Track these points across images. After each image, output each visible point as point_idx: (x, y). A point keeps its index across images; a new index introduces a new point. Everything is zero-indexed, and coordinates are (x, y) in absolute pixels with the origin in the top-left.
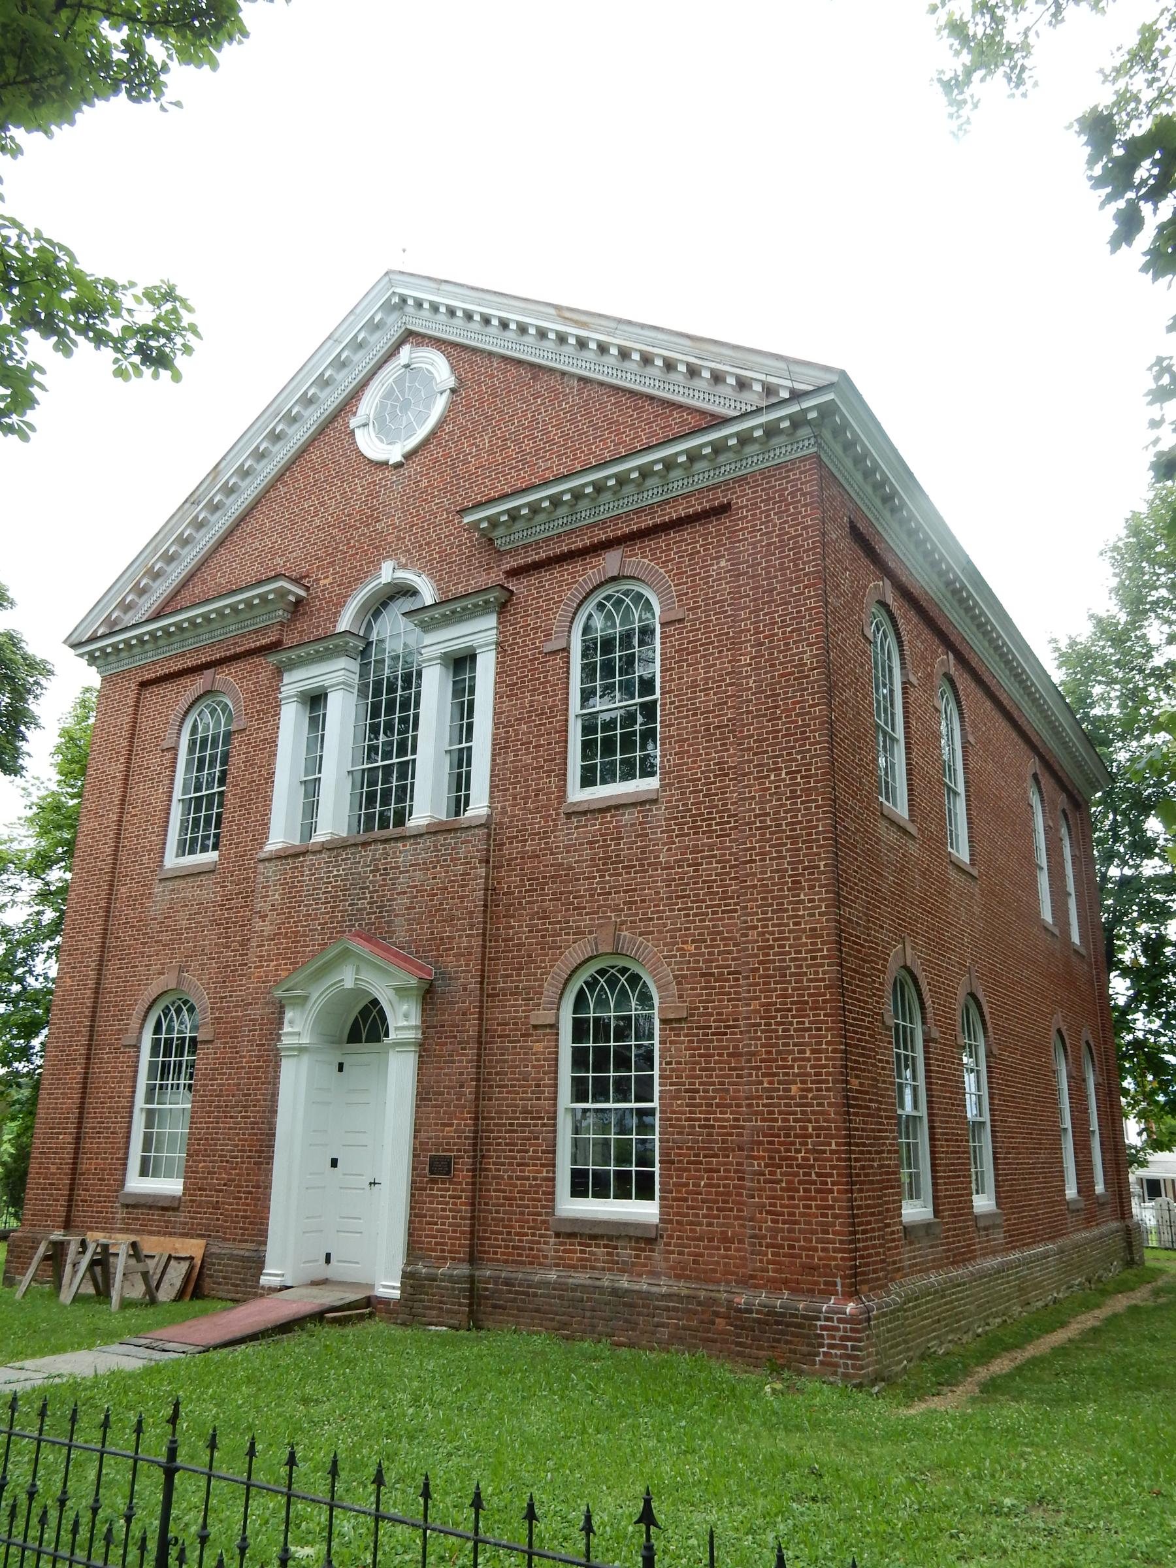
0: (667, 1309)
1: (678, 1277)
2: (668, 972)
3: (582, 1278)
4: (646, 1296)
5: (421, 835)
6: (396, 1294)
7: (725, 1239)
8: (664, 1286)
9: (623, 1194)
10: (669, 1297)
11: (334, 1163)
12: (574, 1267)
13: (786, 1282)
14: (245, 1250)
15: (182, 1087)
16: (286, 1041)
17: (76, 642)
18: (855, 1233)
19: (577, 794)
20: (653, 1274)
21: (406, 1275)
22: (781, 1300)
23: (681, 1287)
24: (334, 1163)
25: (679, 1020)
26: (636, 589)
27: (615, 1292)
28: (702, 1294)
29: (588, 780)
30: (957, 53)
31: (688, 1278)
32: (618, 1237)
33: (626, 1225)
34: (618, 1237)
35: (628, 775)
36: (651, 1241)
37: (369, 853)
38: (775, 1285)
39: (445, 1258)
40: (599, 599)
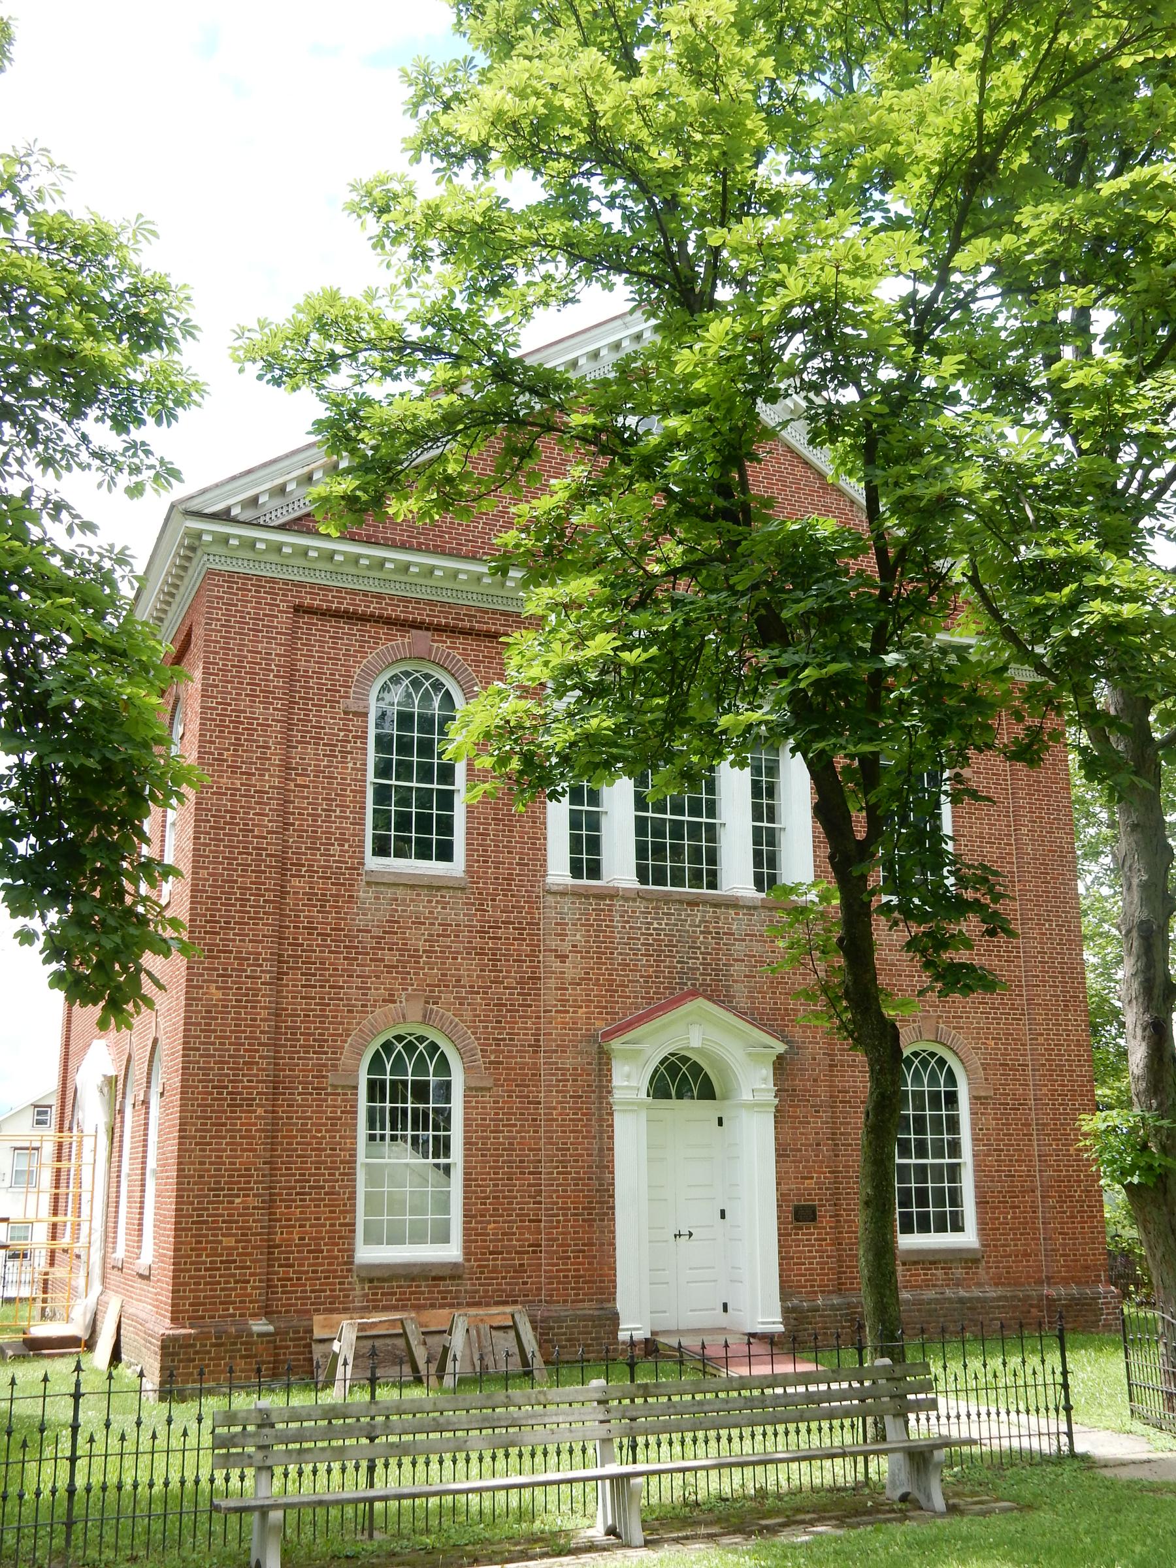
0: (998, 1307)
1: (996, 1285)
2: (976, 1061)
3: (930, 1294)
4: (984, 1300)
5: (755, 908)
6: (780, 1328)
7: (1026, 1255)
8: (992, 1293)
9: (941, 1228)
10: (999, 1299)
11: (723, 1214)
12: (920, 1287)
13: (1072, 1278)
14: (588, 1308)
15: (388, 1138)
16: (617, 1095)
17: (194, 509)
18: (269, 1234)
19: (457, 867)
20: (979, 1285)
21: (786, 1311)
22: (1074, 1290)
23: (999, 1292)
24: (723, 1214)
25: (986, 1098)
26: (437, 676)
27: (961, 1300)
28: (1021, 1295)
29: (446, 853)
30: (609, 287)
31: (1003, 1284)
32: (951, 1261)
33: (960, 1251)
34: (951, 1261)
35: (424, 854)
36: (976, 1261)
37: (698, 914)
38: (1066, 1281)
39: (815, 1292)
40: (397, 671)
